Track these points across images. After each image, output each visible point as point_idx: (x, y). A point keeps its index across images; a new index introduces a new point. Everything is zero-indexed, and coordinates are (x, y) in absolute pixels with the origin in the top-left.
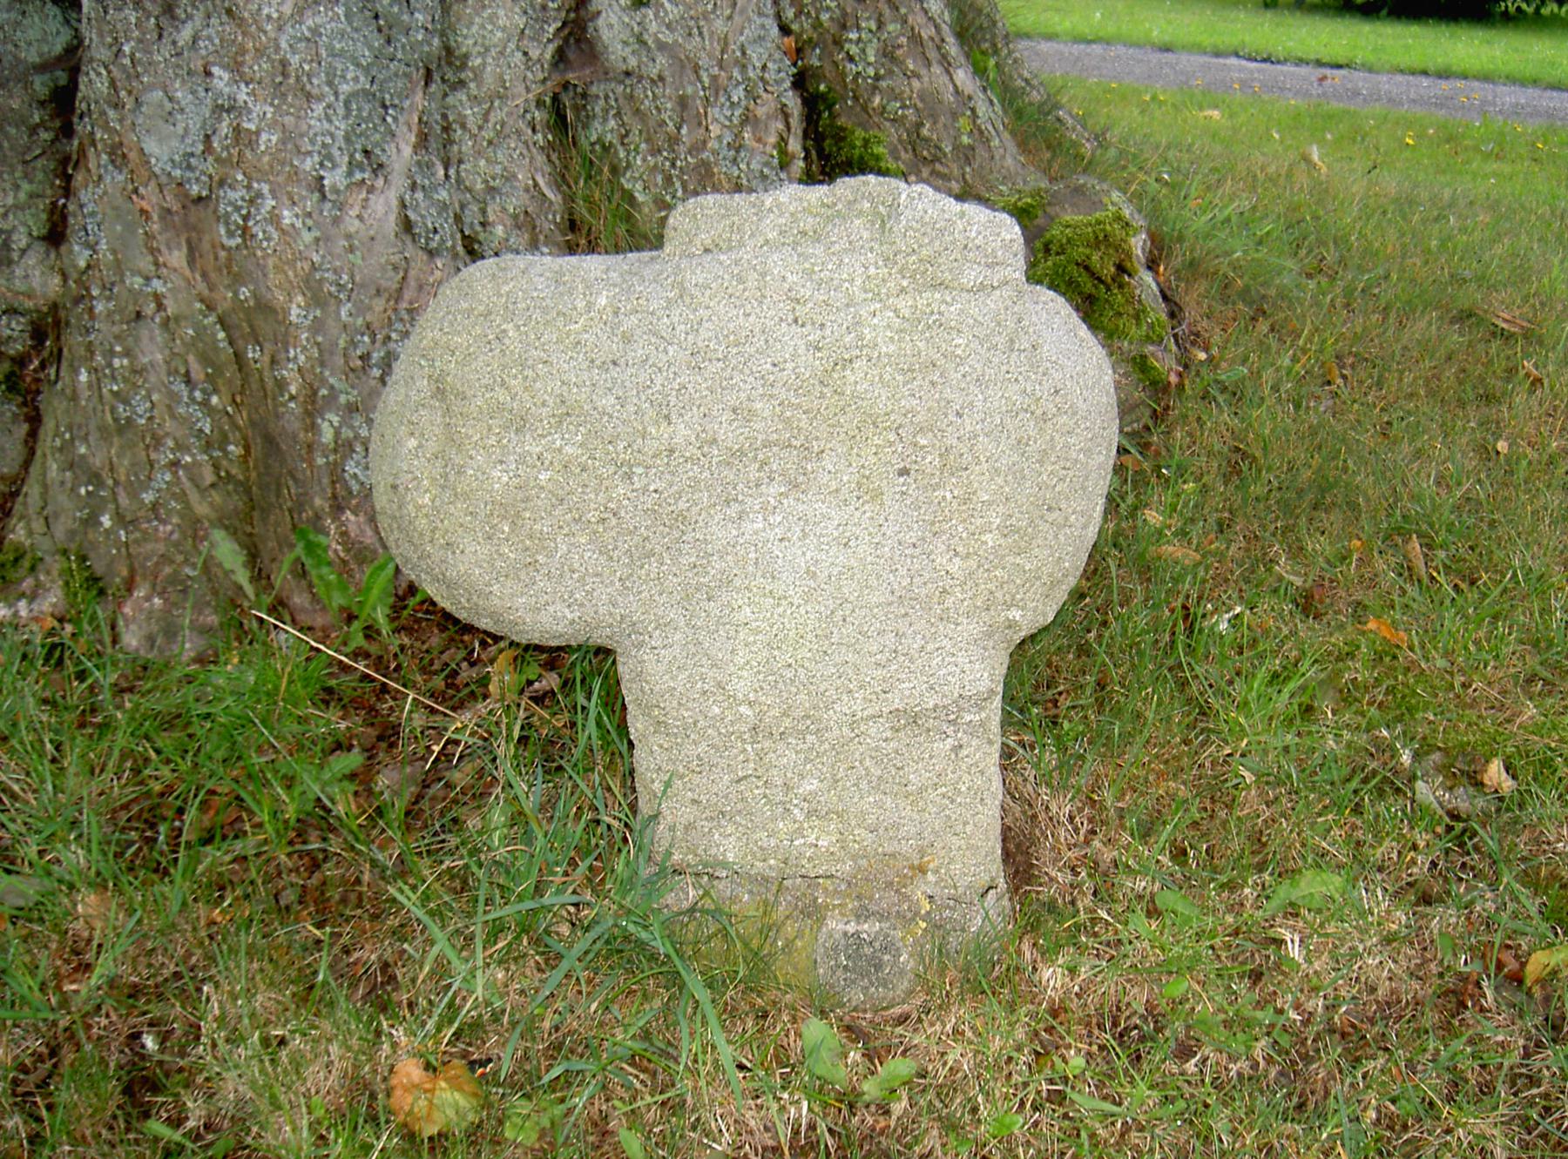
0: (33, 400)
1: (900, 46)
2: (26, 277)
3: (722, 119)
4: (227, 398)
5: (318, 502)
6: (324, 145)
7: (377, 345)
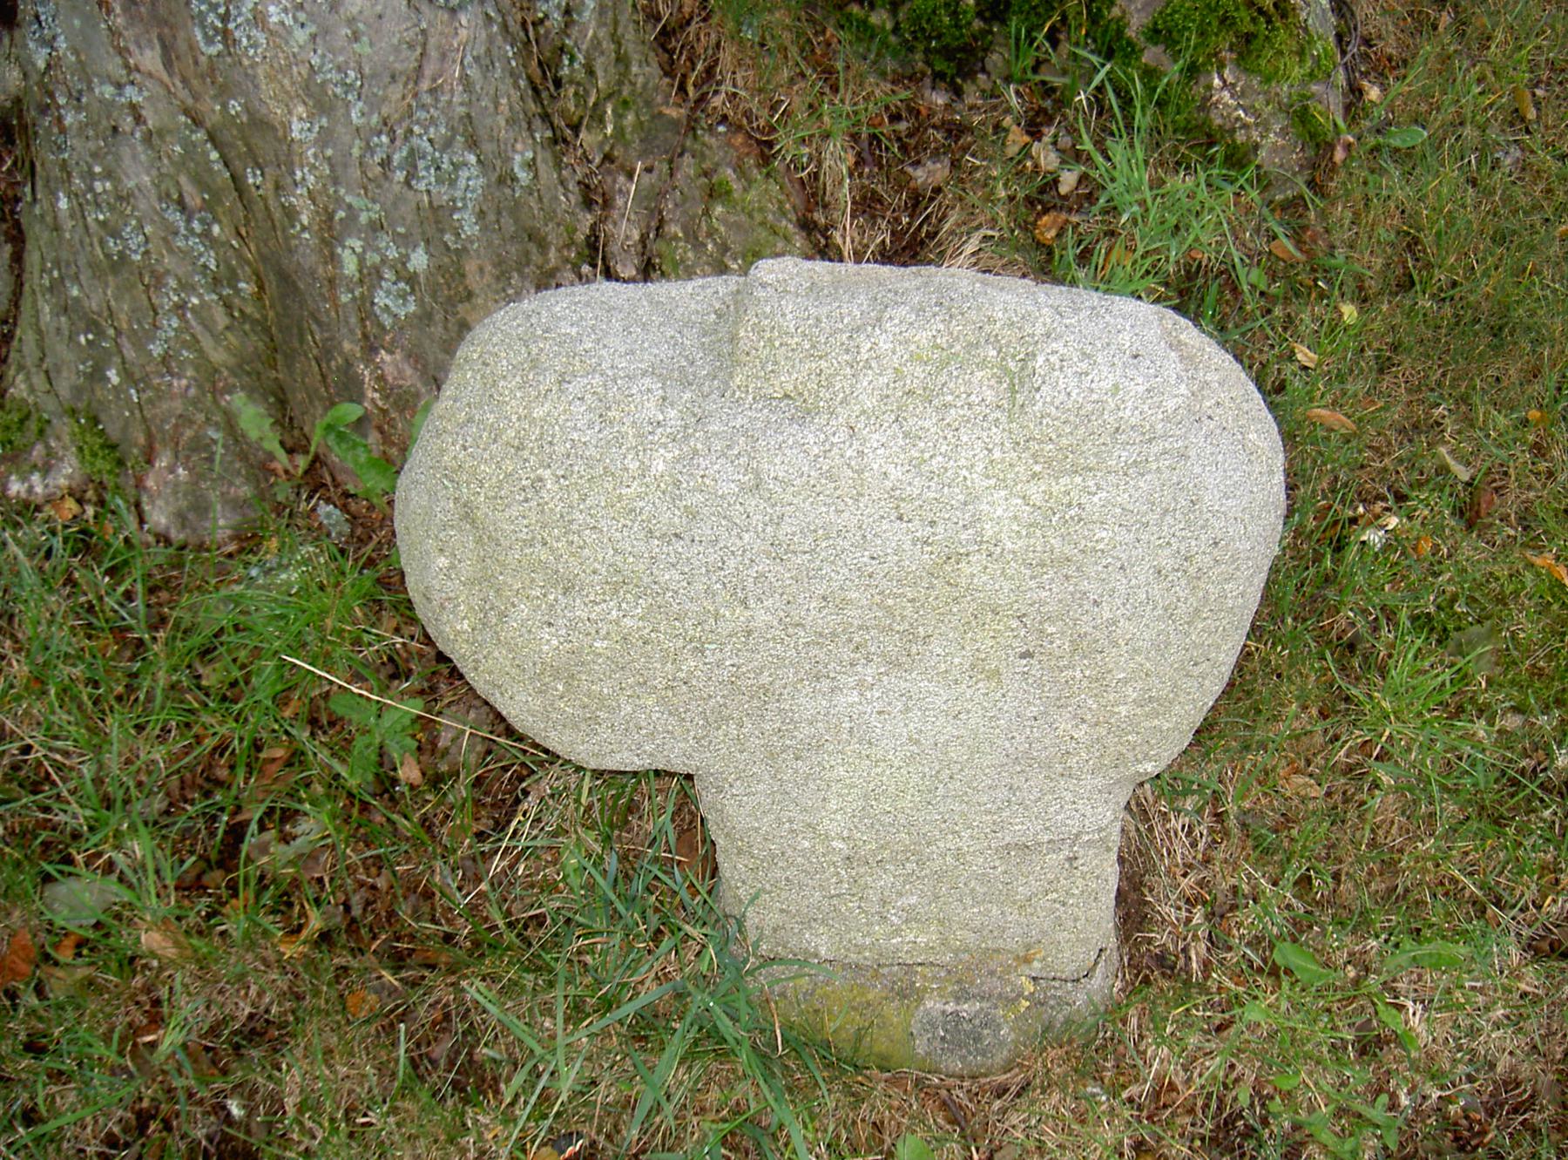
5: (347, 346)
7: (398, 143)
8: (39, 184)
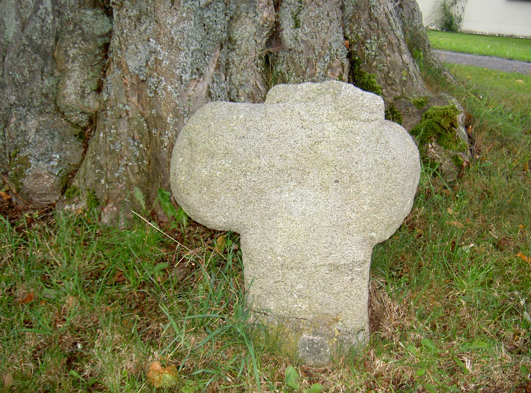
0: (87, 141)
1: (384, 46)
2: (88, 102)
3: (321, 67)
4: (145, 145)
6: (184, 66)
8: (97, 130)
